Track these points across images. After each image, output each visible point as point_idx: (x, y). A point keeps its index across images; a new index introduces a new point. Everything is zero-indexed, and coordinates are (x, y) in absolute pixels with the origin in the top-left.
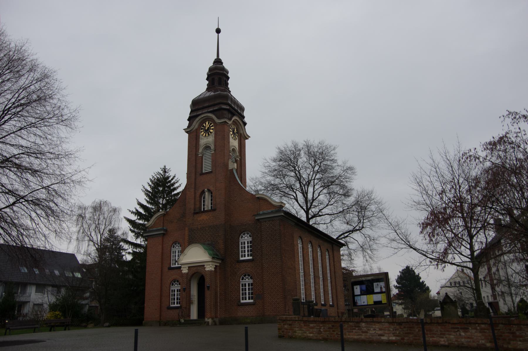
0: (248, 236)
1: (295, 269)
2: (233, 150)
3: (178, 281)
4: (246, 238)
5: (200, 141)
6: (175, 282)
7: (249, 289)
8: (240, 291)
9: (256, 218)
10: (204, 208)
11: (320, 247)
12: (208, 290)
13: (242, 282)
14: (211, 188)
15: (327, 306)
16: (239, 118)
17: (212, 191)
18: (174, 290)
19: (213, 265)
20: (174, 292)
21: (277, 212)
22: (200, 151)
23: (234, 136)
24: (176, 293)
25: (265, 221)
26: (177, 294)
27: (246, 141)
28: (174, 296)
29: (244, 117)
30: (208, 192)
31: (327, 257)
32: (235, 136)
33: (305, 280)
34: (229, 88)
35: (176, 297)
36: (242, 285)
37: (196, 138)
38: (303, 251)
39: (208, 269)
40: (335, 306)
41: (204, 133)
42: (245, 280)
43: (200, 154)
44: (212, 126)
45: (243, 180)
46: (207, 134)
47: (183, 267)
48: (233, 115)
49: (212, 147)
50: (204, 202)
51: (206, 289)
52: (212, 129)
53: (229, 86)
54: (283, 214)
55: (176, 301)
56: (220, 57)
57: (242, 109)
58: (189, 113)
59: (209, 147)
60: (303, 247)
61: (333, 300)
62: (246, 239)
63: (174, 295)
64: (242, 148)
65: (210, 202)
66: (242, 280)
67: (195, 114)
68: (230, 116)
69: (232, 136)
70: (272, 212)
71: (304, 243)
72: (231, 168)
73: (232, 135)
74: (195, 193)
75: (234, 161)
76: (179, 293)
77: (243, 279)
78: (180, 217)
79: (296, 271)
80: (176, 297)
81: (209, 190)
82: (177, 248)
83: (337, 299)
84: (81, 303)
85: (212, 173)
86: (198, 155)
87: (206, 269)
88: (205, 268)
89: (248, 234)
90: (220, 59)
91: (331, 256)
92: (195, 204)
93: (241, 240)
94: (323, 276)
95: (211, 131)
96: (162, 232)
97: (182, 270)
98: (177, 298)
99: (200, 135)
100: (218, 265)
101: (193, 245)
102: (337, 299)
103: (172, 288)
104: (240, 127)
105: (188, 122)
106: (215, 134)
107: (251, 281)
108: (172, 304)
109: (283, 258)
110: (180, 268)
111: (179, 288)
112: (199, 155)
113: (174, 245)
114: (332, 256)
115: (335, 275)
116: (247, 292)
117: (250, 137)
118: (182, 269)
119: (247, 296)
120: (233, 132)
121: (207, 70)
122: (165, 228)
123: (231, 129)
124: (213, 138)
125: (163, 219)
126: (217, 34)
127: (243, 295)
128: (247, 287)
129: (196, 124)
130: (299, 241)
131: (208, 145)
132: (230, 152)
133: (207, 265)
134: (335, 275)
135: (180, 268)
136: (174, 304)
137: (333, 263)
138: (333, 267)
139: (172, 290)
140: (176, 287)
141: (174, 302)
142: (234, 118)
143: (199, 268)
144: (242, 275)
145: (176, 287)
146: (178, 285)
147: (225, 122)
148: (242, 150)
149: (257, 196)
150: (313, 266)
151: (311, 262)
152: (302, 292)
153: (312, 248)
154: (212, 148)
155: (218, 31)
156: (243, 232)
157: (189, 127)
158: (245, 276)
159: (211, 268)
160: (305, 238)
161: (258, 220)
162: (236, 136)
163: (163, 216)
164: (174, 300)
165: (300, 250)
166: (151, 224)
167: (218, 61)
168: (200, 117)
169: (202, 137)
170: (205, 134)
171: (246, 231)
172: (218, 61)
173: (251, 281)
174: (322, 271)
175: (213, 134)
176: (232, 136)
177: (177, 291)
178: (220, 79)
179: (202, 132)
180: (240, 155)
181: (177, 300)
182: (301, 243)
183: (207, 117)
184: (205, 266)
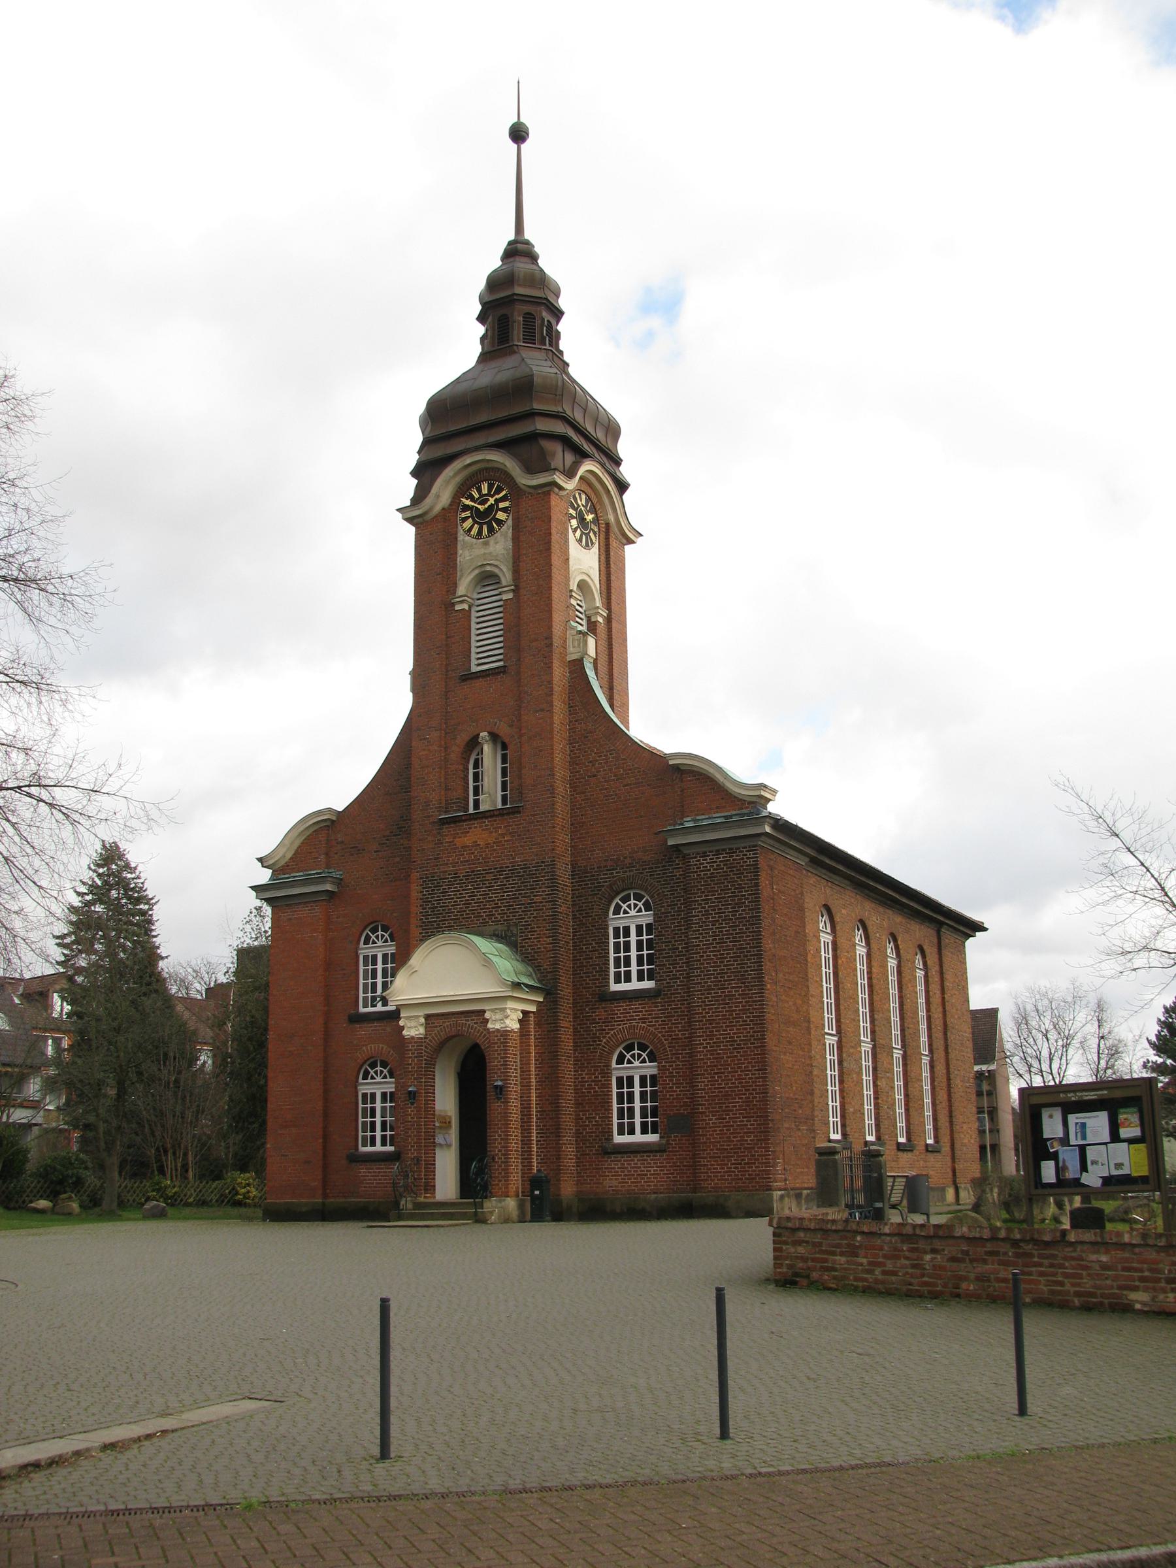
0: (640, 905)
1: (808, 1027)
2: (583, 585)
3: (384, 1064)
4: (633, 913)
5: (460, 552)
6: (373, 1065)
7: (643, 1095)
8: (609, 1103)
10: (477, 804)
11: (895, 940)
14: (504, 730)
15: (916, 1152)
16: (603, 465)
17: (506, 740)
18: (373, 1095)
19: (516, 1010)
20: (373, 1100)
23: (582, 533)
24: (378, 1105)
25: (704, 855)
26: (384, 1109)
27: (628, 548)
28: (373, 1115)
29: (617, 462)
30: (491, 745)
31: (920, 974)
32: (587, 535)
33: (840, 1062)
34: (561, 353)
35: (378, 1120)
36: (620, 1080)
38: (835, 957)
40: (946, 1148)
41: (475, 522)
42: (629, 1062)
45: (616, 696)
46: (485, 528)
47: (408, 1018)
48: (583, 455)
49: (506, 577)
50: (476, 777)
51: (491, 1095)
52: (504, 510)
53: (563, 345)
55: (378, 1133)
56: (528, 235)
57: (613, 430)
58: (417, 449)
59: (493, 576)
60: (834, 943)
61: (936, 1128)
63: (373, 1110)
64: (613, 578)
65: (499, 779)
67: (440, 451)
68: (570, 458)
69: (578, 533)
70: (729, 824)
71: (838, 928)
72: (574, 657)
73: (575, 531)
75: (584, 629)
76: (388, 1104)
77: (620, 1061)
79: (813, 1032)
80: (378, 1120)
81: (494, 737)
82: (380, 943)
83: (951, 1123)
85: (504, 672)
86: (453, 605)
87: (490, 1026)
88: (487, 1021)
89: (638, 897)
90: (527, 243)
91: (934, 971)
94: (904, 1046)
95: (501, 516)
97: (403, 1028)
98: (384, 1124)
99: (461, 532)
100: (533, 1008)
101: (439, 939)
102: (951, 1123)
103: (365, 951)
106: (516, 528)
107: (651, 1069)
108: (364, 1145)
109: (769, 986)
110: (395, 1015)
111: (390, 1088)
112: (457, 607)
113: (366, 1070)
114: (937, 968)
115: (946, 1039)
116: (637, 1105)
118: (401, 1023)
119: (638, 1120)
120: (582, 520)
121: (481, 284)
124: (510, 544)
126: (516, 146)
127: (621, 1115)
128: (637, 1089)
129: (443, 492)
130: (823, 923)
131: (488, 568)
132: (571, 596)
133: (492, 1010)
134: (946, 1039)
135: (395, 1015)
136: (373, 1144)
137: (938, 992)
138: (940, 1009)
139: (364, 1095)
140: (378, 1085)
141: (373, 1138)
142: (587, 466)
143: (463, 1020)
144: (618, 1046)
145: (378, 1085)
146: (385, 1077)
148: (614, 584)
150: (872, 1011)
151: (863, 996)
152: (830, 1103)
153: (868, 943)
154: (504, 583)
155: (518, 134)
156: (621, 889)
157: (417, 499)
158: (629, 1048)
160: (844, 911)
161: (677, 847)
162: (591, 534)
164: (373, 1129)
165: (826, 955)
169: (467, 538)
173: (651, 1069)
174: (902, 1026)
175: (508, 529)
176: (578, 533)
177: (384, 1099)
178: (529, 318)
179: (464, 520)
180: (608, 605)
181: (384, 1129)
182: (829, 930)
183: (482, 465)
184: (487, 1015)
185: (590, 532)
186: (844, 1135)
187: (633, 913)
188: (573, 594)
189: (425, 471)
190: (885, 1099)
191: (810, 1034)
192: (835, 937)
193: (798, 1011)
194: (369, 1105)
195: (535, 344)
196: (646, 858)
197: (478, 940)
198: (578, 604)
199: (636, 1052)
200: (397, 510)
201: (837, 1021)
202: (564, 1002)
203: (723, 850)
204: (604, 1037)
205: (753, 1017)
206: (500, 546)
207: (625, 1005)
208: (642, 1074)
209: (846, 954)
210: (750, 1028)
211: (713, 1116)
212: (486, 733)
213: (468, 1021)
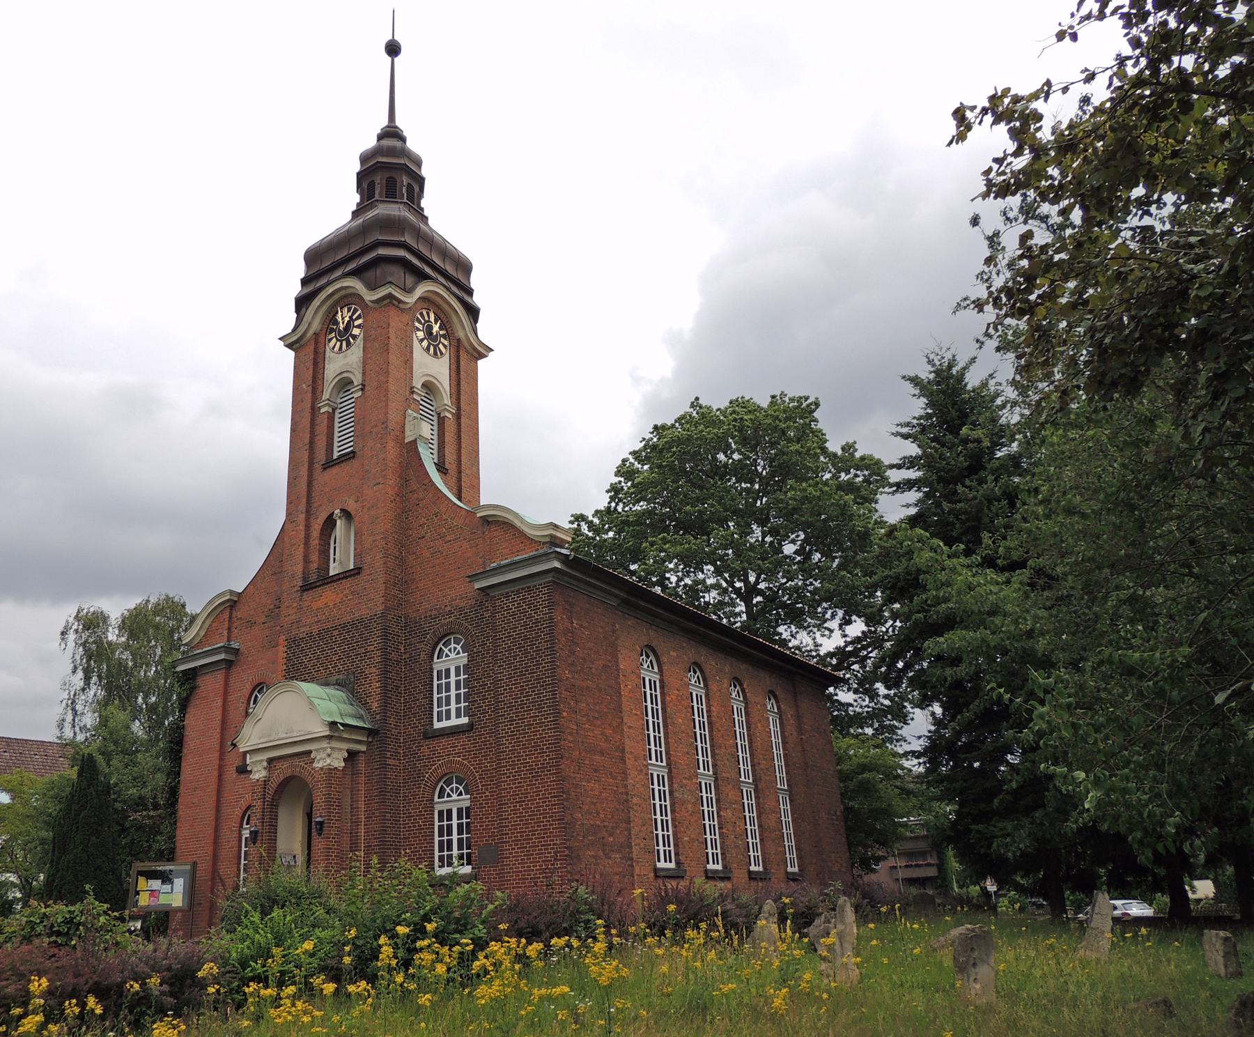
9: (477, 586)
12: (320, 835)
13: (440, 805)
14: (351, 506)
19: (340, 750)
21: (545, 557)
22: (326, 395)
25: (507, 596)
27: (481, 363)
29: (470, 292)
37: (315, 359)
39: (320, 765)
41: (337, 340)
43: (324, 406)
44: (359, 318)
52: (359, 326)
54: (557, 564)
56: (399, 122)
62: (453, 658)
66: (439, 798)
67: (310, 288)
68: (410, 280)
73: (422, 340)
74: (308, 527)
78: (272, 607)
81: (347, 515)
84: (460, 872)
86: (319, 408)
88: (313, 761)
89: (457, 642)
90: (396, 127)
92: (306, 560)
93: (438, 665)
95: (356, 331)
96: (222, 656)
99: (328, 349)
104: (455, 319)
105: (291, 354)
106: (365, 340)
107: (465, 801)
109: (565, 714)
112: (322, 411)
113: (256, 695)
116: (455, 837)
117: (492, 350)
122: (235, 645)
123: (419, 322)
125: (230, 618)
126: (390, 59)
131: (345, 375)
132: (413, 392)
133: (317, 750)
143: (296, 761)
147: (390, 296)
149: (478, 515)
154: (356, 384)
155: (393, 49)
156: (442, 637)
159: (328, 761)
163: (231, 606)
166: (197, 634)
167: (391, 133)
168: (323, 295)
169: (332, 354)
170: (338, 343)
171: (453, 633)
172: (391, 133)
173: (465, 801)
175: (360, 341)
179: (418, 329)
183: (343, 293)
185: (439, 344)
186: (678, 863)
187: (453, 656)
188: (415, 390)
189: (302, 303)
190: (731, 829)
191: (625, 763)
192: (661, 675)
193: (607, 740)
194: (445, 853)
195: (396, 198)
196: (461, 605)
197: (303, 685)
198: (422, 400)
199: (454, 785)
200: (280, 339)
201: (666, 754)
202: (392, 742)
203: (523, 589)
204: (427, 773)
205: (549, 744)
206: (354, 356)
207: (444, 741)
208: (460, 806)
209: (677, 692)
210: (547, 756)
211: (515, 845)
212: (338, 511)
213: (300, 762)
